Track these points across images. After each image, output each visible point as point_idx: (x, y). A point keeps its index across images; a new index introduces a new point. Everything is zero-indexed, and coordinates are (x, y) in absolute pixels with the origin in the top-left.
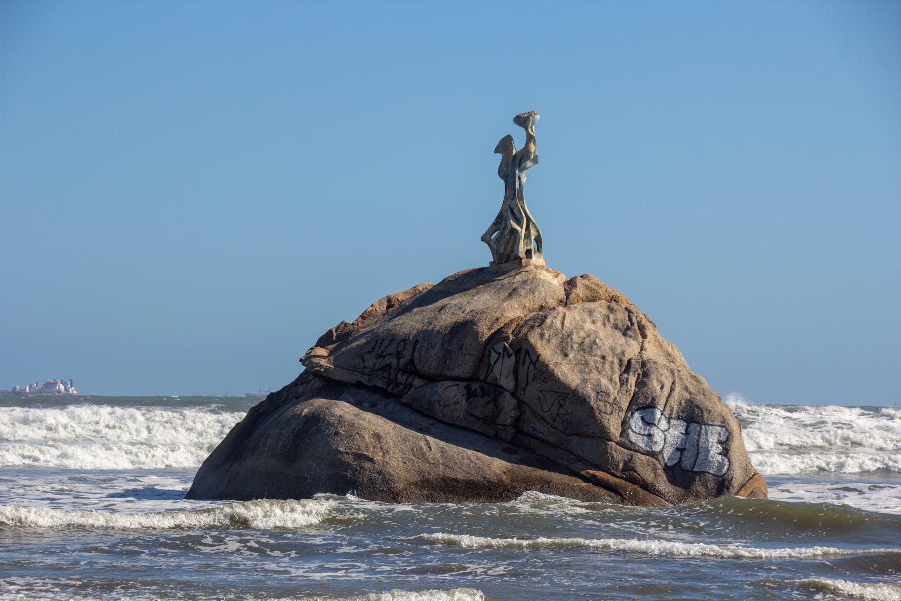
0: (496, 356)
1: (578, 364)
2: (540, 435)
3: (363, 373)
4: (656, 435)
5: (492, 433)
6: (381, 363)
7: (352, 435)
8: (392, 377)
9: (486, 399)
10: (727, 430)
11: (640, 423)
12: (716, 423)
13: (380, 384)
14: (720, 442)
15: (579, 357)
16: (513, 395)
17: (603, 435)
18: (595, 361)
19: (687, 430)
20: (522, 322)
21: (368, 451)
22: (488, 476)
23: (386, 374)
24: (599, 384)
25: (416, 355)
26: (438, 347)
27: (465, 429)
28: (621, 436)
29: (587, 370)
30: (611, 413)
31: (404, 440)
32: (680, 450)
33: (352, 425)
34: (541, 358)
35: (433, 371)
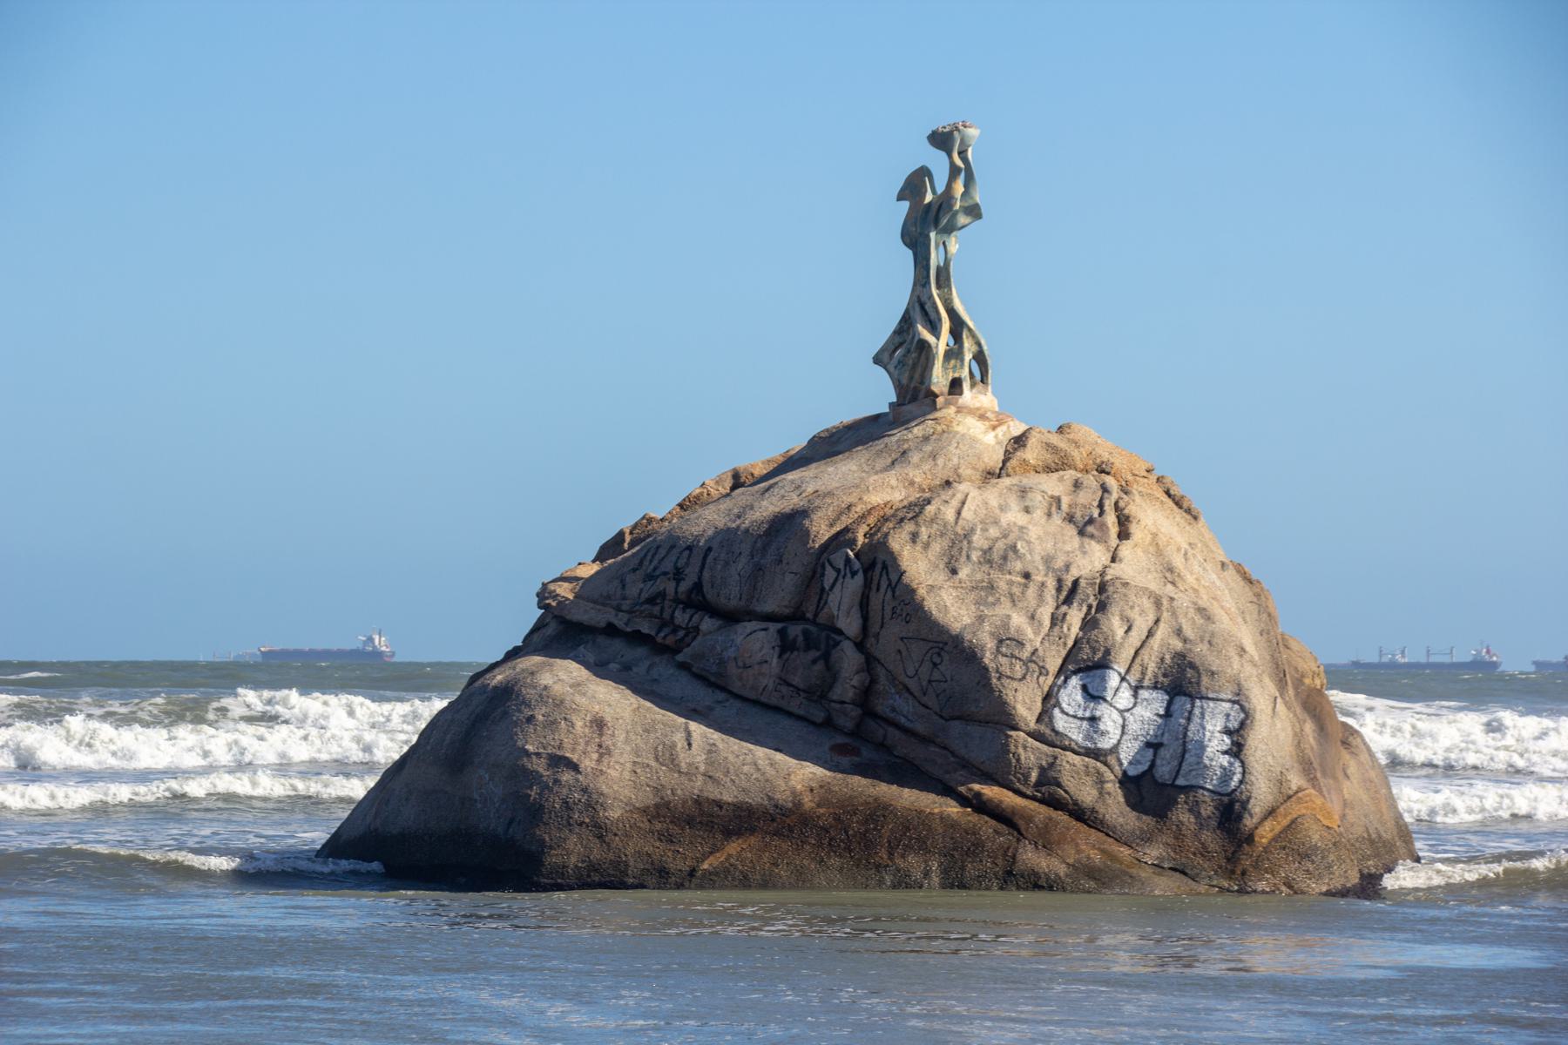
0: (834, 574)
1: (974, 588)
2: (903, 720)
3: (618, 609)
4: (1106, 719)
5: (819, 716)
6: (650, 589)
7: (554, 722)
8: (666, 615)
9: (814, 654)
10: (1243, 708)
11: (1079, 696)
13: (646, 628)
14: (1227, 732)
15: (979, 576)
16: (860, 646)
17: (1004, 720)
18: (1010, 583)
19: (1168, 709)
20: (889, 512)
21: (574, 750)
22: (778, 796)
23: (656, 610)
24: (1006, 625)
25: (706, 574)
26: (743, 560)
27: (777, 709)
28: (1039, 720)
29: (991, 599)
30: (1024, 678)
31: (647, 731)
32: (1153, 746)
33: (559, 703)
34: (906, 579)
35: (734, 603)
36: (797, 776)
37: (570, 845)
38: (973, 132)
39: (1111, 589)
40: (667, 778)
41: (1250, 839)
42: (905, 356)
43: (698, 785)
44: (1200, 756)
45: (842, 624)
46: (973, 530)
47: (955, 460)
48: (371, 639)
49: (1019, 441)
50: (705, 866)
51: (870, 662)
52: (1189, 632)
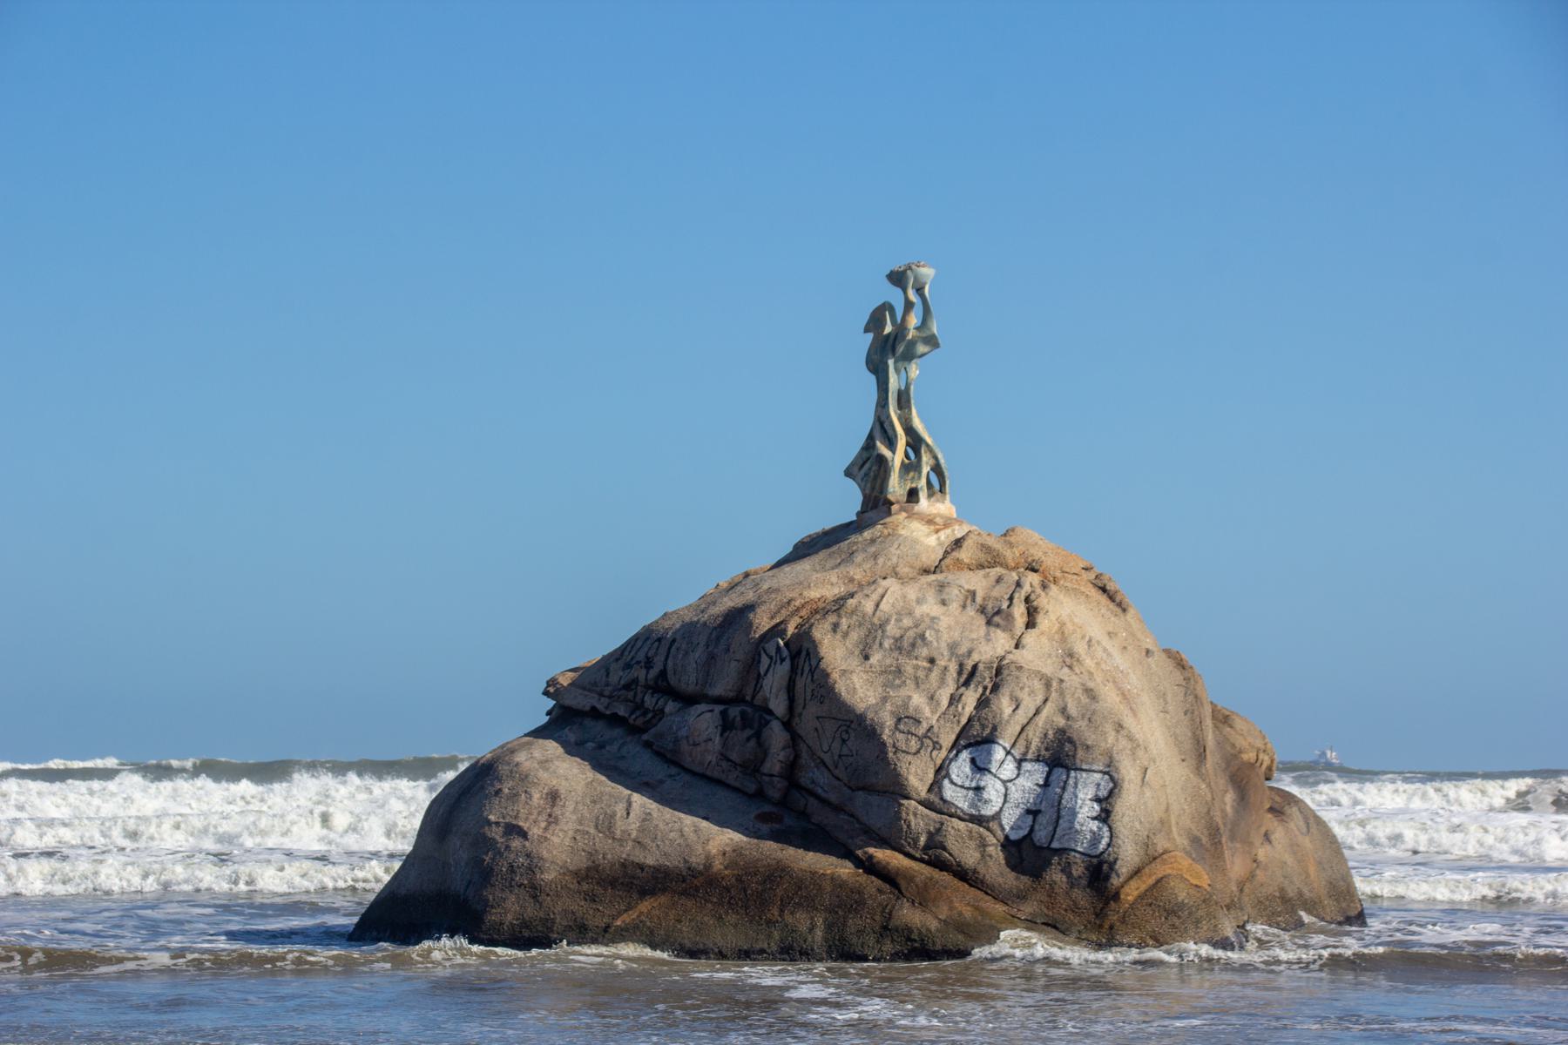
3: (601, 695)
5: (751, 787)
8: (638, 700)
9: (748, 732)
10: (1112, 779)
11: (967, 769)
12: (1095, 767)
13: (622, 711)
14: (1098, 800)
15: (888, 662)
16: (787, 725)
17: (897, 790)
18: (916, 667)
20: (821, 605)
22: (693, 860)
24: (906, 705)
25: (670, 663)
26: (700, 649)
28: (929, 790)
29: (897, 682)
30: (918, 752)
31: (594, 802)
32: (1033, 812)
33: (524, 778)
34: (823, 665)
36: (714, 840)
37: (508, 904)
38: (927, 272)
39: (1005, 672)
40: (602, 844)
41: (1116, 897)
42: (869, 469)
43: (627, 851)
44: (1072, 822)
45: (772, 705)
46: (887, 621)
47: (895, 560)
48: (1324, 754)
49: (958, 543)
50: (619, 923)
51: (795, 738)
52: (1073, 710)
